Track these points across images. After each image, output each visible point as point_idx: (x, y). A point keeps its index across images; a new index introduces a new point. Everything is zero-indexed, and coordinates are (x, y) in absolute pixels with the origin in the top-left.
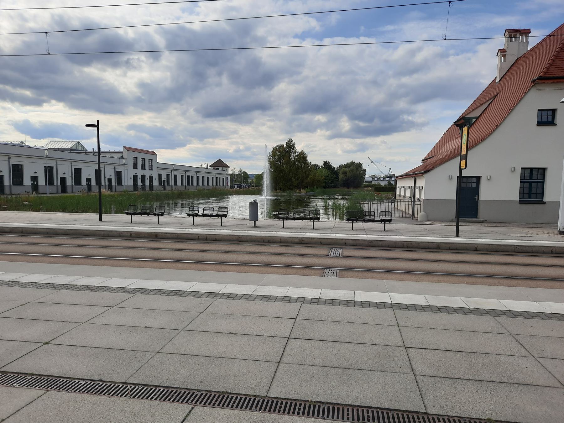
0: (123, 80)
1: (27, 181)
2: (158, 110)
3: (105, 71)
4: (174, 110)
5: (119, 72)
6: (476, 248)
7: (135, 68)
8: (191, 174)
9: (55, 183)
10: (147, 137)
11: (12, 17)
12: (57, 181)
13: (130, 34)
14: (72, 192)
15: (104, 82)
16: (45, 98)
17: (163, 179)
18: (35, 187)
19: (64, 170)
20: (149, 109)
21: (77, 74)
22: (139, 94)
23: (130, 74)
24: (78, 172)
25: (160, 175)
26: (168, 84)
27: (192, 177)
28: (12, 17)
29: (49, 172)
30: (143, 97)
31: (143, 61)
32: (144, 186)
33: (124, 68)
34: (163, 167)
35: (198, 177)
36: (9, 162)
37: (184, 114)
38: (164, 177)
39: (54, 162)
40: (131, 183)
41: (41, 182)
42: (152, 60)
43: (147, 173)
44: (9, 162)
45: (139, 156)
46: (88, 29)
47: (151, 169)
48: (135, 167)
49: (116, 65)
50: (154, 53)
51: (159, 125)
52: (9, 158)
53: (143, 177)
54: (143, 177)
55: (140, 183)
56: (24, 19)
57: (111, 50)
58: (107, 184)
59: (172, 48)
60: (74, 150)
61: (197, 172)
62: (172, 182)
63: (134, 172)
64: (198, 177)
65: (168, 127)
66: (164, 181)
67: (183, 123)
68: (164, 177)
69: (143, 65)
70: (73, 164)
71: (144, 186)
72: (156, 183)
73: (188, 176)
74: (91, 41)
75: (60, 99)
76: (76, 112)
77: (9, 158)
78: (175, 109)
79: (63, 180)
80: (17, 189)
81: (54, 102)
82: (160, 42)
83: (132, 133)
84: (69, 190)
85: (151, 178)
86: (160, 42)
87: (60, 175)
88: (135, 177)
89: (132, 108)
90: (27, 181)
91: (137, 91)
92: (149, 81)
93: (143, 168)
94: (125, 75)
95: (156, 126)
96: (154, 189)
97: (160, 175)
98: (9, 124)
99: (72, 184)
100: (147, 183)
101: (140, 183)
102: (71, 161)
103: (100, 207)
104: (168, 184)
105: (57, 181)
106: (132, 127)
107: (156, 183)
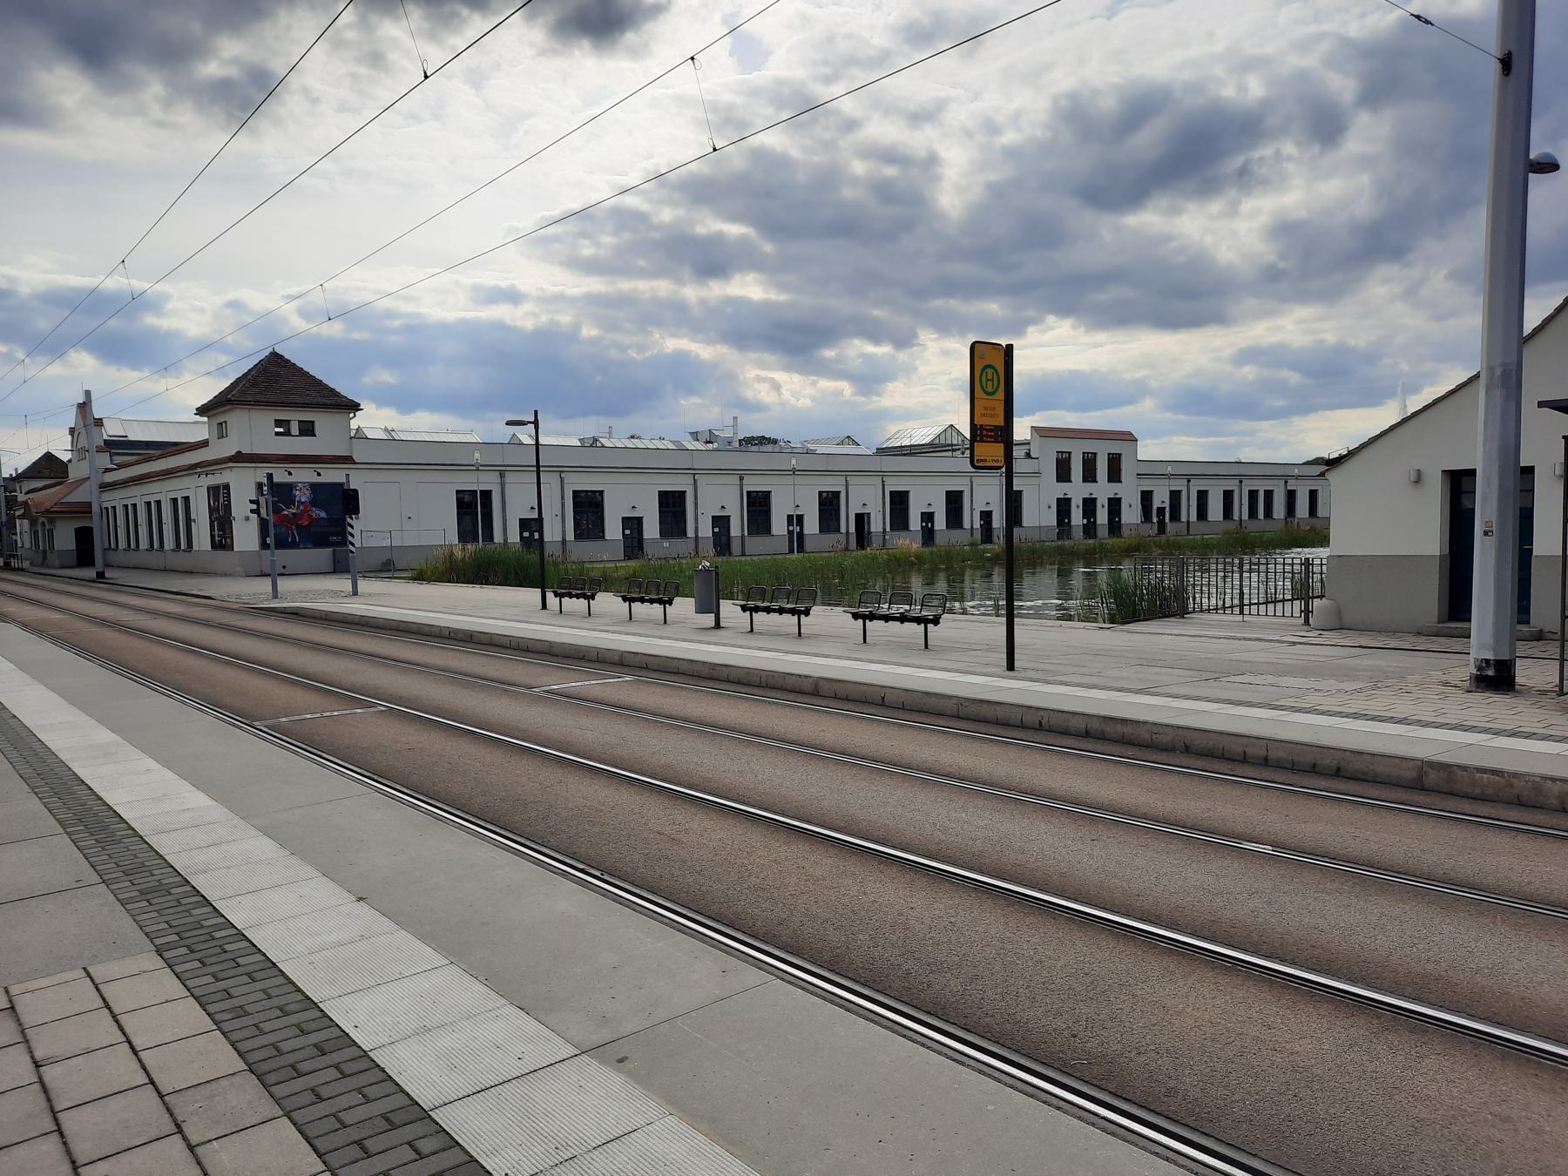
0: (1219, 230)
1: (614, 530)
2: (1330, 296)
3: (1176, 211)
4: (1381, 287)
5: (1216, 206)
6: (1266, 758)
7: (1265, 182)
8: (1261, 487)
9: (967, 525)
10: (1294, 378)
11: (969, 134)
12: (848, 524)
13: (1256, 88)
14: (743, 554)
15: (1174, 244)
16: (1031, 313)
17: (1156, 504)
18: (798, 540)
19: (866, 499)
20: (1302, 296)
21: (1107, 235)
22: (1271, 257)
23: (1248, 205)
24: (899, 502)
25: (1147, 497)
26: (1365, 208)
27: (1269, 494)
28: (969, 134)
29: (829, 505)
30: (1282, 265)
31: (1289, 158)
32: (1090, 529)
33: (1233, 192)
34: (1155, 470)
35: (1291, 496)
36: (741, 486)
37: (1411, 293)
38: (1161, 499)
39: (842, 480)
40: (1051, 519)
41: (812, 526)
42: (1316, 149)
43: (1102, 490)
44: (741, 486)
45: (1102, 451)
46: (1141, 106)
47: (1114, 475)
48: (1063, 474)
49: (1208, 188)
50: (1325, 125)
51: (1330, 338)
52: (741, 479)
53: (1089, 505)
54: (1089, 505)
55: (1077, 518)
56: (991, 128)
57: (1195, 146)
58: (977, 525)
59: (1375, 94)
60: (937, 446)
61: (1286, 478)
62: (1189, 511)
63: (1062, 490)
64: (1291, 496)
65: (1360, 339)
66: (1161, 511)
67: (1412, 321)
68: (1161, 499)
69: (1291, 167)
70: (888, 481)
71: (1090, 529)
72: (1131, 515)
73: (1253, 495)
74: (1147, 141)
75: (1063, 310)
76: (1101, 337)
77: (741, 479)
78: (1386, 281)
79: (861, 519)
80: (757, 544)
81: (1051, 319)
82: (1343, 86)
83: (1249, 372)
84: (736, 547)
85: (1115, 505)
86: (1343, 86)
87: (855, 508)
88: (1063, 506)
89: (1250, 302)
90: (779, 526)
91: (1266, 252)
92: (1303, 214)
93: (1089, 475)
94: (1233, 211)
95: (1322, 341)
96: (1125, 531)
97: (1147, 497)
98: (954, 389)
99: (564, 541)
100: (1102, 517)
101: (1077, 518)
102: (882, 474)
103: (649, 586)
104: (1175, 516)
105: (848, 524)
106: (1249, 355)
107: (1131, 515)
